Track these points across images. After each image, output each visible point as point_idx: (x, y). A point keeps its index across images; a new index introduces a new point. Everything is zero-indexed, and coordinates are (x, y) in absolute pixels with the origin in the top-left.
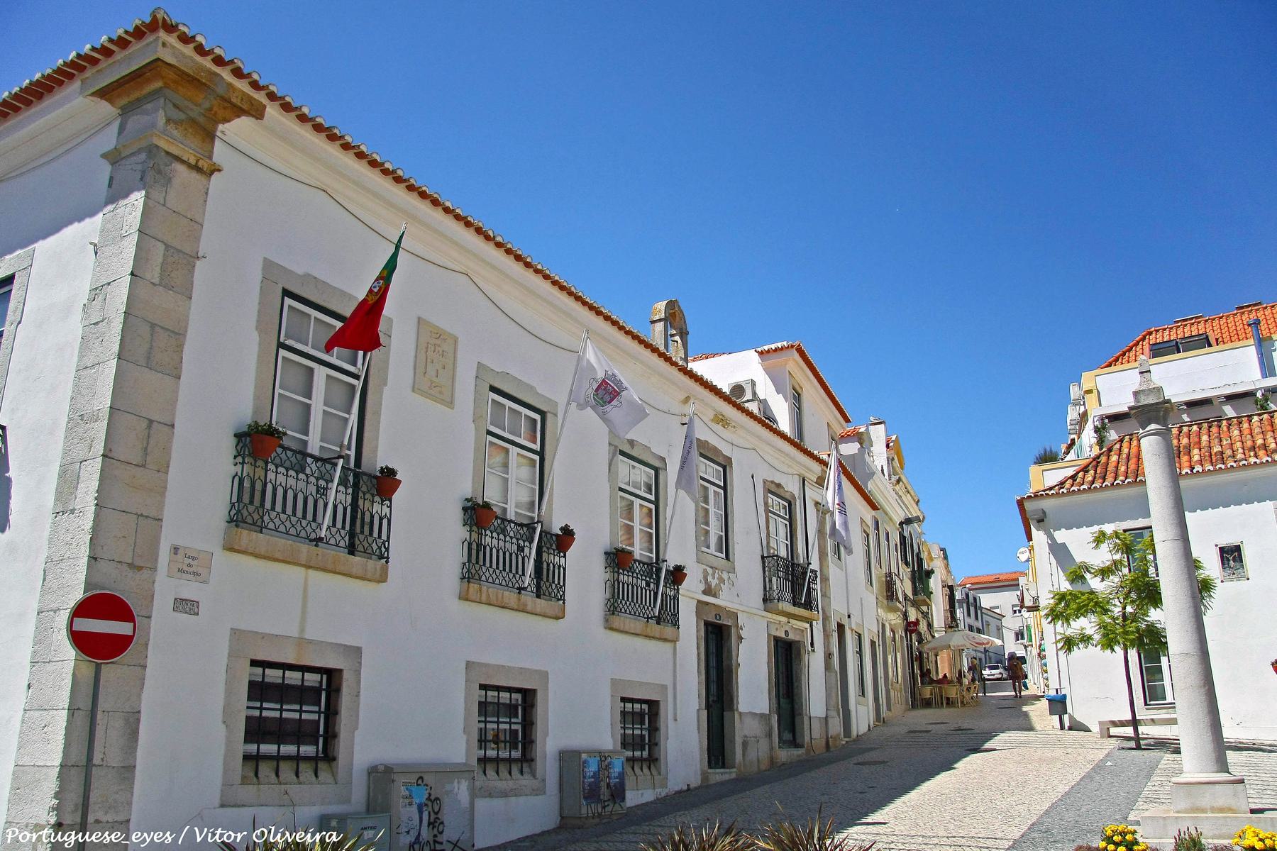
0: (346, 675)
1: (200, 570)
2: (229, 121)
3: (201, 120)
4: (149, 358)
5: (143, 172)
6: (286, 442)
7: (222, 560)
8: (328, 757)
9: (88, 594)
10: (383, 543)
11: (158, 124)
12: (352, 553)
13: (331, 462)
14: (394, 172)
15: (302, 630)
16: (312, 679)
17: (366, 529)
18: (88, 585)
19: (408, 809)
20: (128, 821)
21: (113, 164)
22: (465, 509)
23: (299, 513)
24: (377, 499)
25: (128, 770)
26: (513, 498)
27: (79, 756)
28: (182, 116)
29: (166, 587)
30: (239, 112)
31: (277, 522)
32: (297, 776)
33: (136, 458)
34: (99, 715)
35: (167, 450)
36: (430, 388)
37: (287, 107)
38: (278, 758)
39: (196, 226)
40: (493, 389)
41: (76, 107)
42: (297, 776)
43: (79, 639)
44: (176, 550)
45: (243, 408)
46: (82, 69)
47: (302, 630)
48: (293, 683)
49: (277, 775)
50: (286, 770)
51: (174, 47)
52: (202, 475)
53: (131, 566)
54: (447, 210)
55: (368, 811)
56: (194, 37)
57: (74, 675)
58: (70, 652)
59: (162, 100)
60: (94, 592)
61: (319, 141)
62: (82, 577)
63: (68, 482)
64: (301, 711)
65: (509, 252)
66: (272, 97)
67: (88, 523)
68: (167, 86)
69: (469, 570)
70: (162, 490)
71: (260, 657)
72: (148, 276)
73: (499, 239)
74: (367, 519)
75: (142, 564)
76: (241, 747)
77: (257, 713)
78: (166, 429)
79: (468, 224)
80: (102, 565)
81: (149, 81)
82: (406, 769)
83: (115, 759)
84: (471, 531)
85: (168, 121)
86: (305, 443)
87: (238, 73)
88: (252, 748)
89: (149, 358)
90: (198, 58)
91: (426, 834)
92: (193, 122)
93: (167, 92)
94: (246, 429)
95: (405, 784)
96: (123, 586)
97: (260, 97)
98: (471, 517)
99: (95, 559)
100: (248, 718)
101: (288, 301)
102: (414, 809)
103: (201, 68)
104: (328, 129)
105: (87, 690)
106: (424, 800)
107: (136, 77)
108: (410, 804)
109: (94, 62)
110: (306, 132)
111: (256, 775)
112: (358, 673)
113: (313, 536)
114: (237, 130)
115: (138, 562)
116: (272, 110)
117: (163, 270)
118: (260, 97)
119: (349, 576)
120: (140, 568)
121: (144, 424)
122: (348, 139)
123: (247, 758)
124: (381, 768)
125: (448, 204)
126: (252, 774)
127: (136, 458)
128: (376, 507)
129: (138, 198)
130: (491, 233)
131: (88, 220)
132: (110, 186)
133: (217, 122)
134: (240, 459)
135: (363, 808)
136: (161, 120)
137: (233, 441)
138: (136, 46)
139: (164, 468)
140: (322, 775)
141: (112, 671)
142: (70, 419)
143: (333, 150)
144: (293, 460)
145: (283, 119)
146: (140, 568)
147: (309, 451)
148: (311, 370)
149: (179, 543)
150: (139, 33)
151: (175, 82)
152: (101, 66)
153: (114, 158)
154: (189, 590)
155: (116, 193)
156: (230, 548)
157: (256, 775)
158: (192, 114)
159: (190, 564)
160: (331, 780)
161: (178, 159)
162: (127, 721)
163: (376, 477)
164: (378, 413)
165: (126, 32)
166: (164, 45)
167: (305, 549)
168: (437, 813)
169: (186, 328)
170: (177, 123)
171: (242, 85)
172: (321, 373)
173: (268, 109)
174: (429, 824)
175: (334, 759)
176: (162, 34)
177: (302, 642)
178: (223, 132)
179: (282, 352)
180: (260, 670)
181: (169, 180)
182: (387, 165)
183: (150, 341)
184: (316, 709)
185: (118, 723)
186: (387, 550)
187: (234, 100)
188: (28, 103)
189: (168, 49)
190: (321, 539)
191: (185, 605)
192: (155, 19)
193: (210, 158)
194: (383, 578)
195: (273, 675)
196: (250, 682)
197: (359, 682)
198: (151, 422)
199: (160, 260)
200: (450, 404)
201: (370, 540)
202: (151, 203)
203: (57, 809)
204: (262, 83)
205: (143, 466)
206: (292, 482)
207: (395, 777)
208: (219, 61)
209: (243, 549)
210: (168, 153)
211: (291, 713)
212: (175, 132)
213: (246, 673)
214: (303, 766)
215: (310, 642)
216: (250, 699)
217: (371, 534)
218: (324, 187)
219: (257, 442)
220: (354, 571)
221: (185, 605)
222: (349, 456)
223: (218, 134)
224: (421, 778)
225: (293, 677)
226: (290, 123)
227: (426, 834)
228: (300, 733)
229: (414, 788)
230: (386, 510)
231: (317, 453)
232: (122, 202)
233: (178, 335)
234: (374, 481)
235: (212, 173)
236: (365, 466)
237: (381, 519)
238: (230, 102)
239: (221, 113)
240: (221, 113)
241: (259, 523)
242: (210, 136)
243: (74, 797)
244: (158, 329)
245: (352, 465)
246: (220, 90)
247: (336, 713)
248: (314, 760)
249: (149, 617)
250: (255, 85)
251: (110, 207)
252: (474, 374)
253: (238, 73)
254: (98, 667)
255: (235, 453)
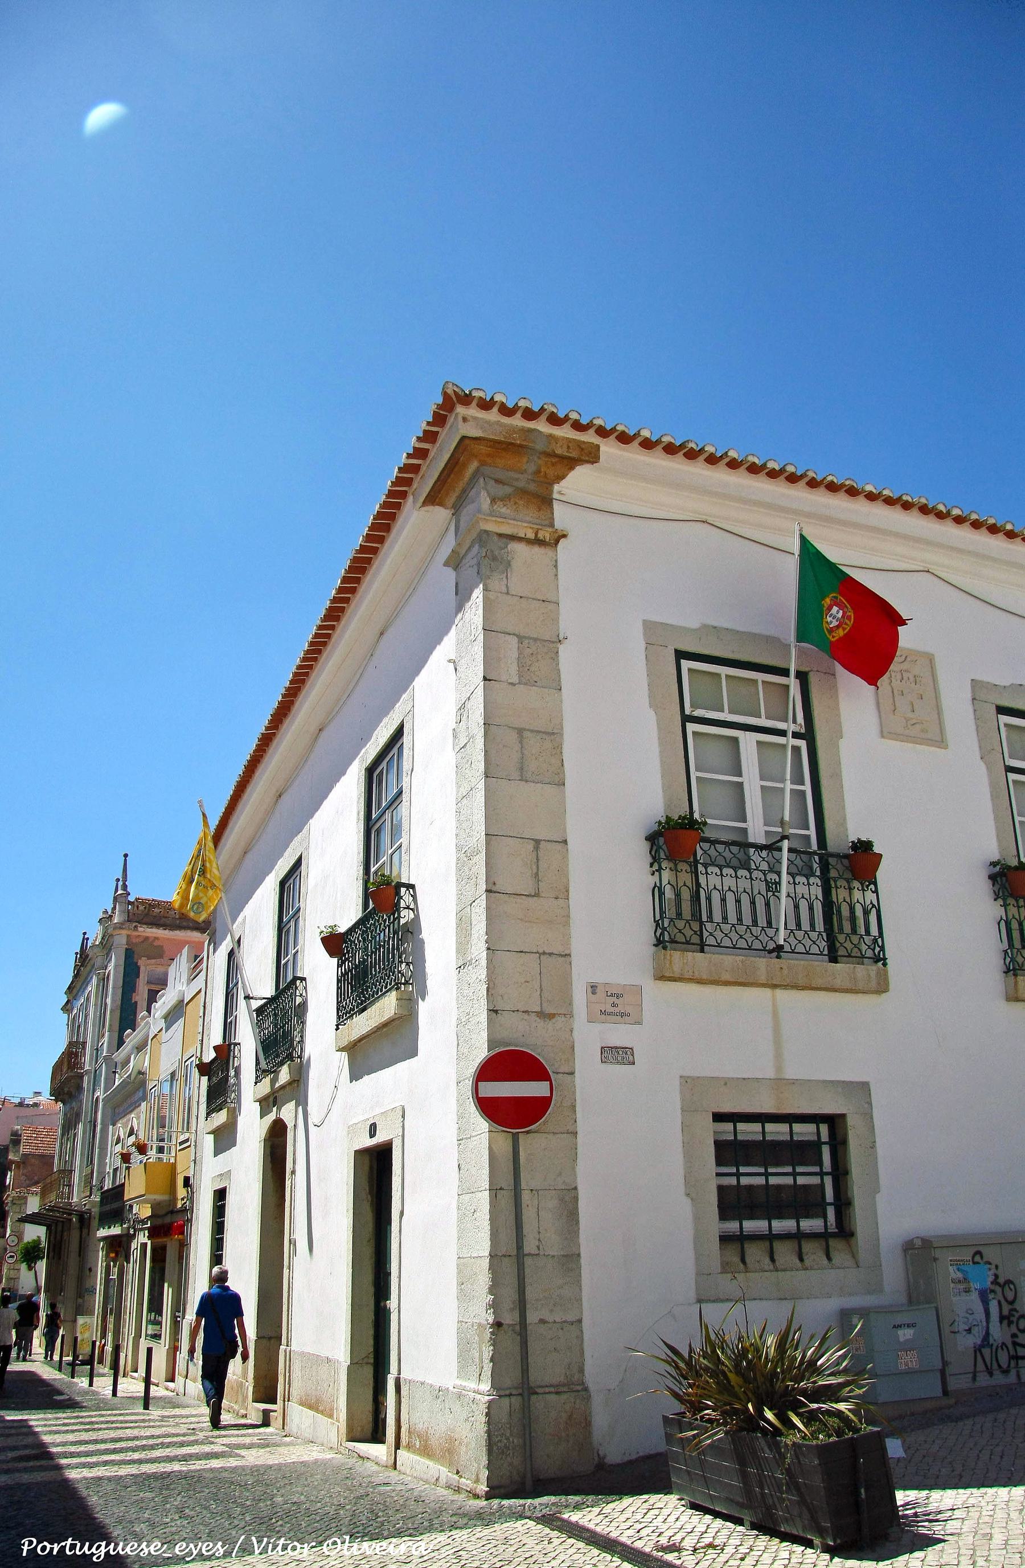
0: (850, 1121)
1: (628, 1009)
2: (563, 477)
3: (532, 487)
4: (522, 769)
5: (479, 564)
6: (708, 833)
7: (657, 996)
8: (845, 1232)
9: (493, 1053)
10: (875, 941)
11: (488, 511)
12: (834, 959)
13: (773, 847)
14: (782, 471)
15: (779, 1068)
16: (804, 1131)
17: (847, 927)
18: (491, 1043)
19: (965, 1297)
20: (580, 1321)
21: (456, 568)
22: (992, 878)
23: (747, 920)
24: (856, 884)
25: (571, 1261)
26: (760, 802)
27: (508, 1246)
28: (508, 490)
29: (588, 1036)
30: (571, 463)
31: (719, 935)
32: (801, 1259)
33: (526, 886)
34: (526, 1196)
35: (563, 872)
36: (906, 727)
37: (624, 438)
38: (770, 1238)
39: (551, 606)
40: (1002, 710)
41: (421, 524)
42: (801, 1259)
43: (489, 1107)
44: (593, 988)
45: (651, 801)
46: (409, 482)
47: (779, 1068)
48: (750, 1138)
49: (773, 1260)
50: (785, 1252)
51: (475, 418)
52: (612, 897)
53: (541, 1015)
54: (871, 497)
55: (910, 1302)
56: (900, 497)
57: (490, 1148)
58: (482, 1125)
59: (482, 480)
60: (497, 1050)
61: (677, 465)
62: (484, 1035)
63: (463, 926)
64: (794, 1174)
65: (976, 525)
66: (603, 432)
67: (483, 974)
68: (483, 463)
69: (1012, 960)
70: (566, 919)
71: (727, 1108)
72: (504, 678)
73: (956, 512)
74: (845, 911)
75: (553, 1012)
76: (715, 1226)
77: (733, 1181)
78: (559, 846)
79: (907, 506)
80: (505, 1019)
81: (465, 466)
82: (953, 1243)
83: (554, 1245)
84: (1005, 905)
85: (493, 500)
86: (745, 831)
87: (554, 420)
88: (733, 1226)
89: (522, 769)
90: (506, 420)
91: (998, 1333)
92: (523, 493)
93: (487, 470)
94: (656, 827)
95: (954, 1263)
96: (534, 1038)
97: (590, 437)
98: (1003, 887)
99: (496, 1012)
100: (721, 1189)
101: (685, 664)
102: (975, 1296)
103: (513, 430)
104: (682, 446)
105: (507, 1167)
106: (988, 1284)
107: (453, 466)
108: (967, 1291)
109: (415, 469)
110: (657, 460)
111: (743, 1260)
112: (868, 1116)
113: (771, 946)
114: (577, 484)
115: (549, 1009)
116: (608, 449)
117: (521, 665)
118: (590, 437)
119: (835, 990)
120: (551, 1016)
121: (531, 846)
122: (710, 449)
123: (725, 1239)
124: (918, 1243)
125: (869, 488)
126: (736, 1259)
127: (526, 886)
128: (857, 895)
129: (478, 594)
130: (941, 507)
131: (446, 639)
132: (457, 594)
133: (551, 484)
134: (656, 867)
135: (903, 1299)
136: (485, 502)
137: (646, 846)
138: (443, 433)
139: (563, 893)
140: (838, 1258)
141: (534, 1143)
142: (458, 859)
143: (698, 470)
144: (727, 854)
145: (626, 454)
146: (551, 1016)
147: (751, 840)
148: (735, 740)
149: (599, 979)
150: (439, 419)
151: (489, 455)
152: (423, 469)
153: (455, 561)
154: (619, 1035)
155: (462, 596)
156: (661, 977)
157: (743, 1260)
158: (521, 484)
159: (615, 1004)
160: (850, 1262)
161: (513, 538)
162: (562, 1200)
163: (846, 856)
164: (837, 776)
165: (428, 423)
166: (465, 420)
167: (762, 964)
168: (1012, 1303)
169: (561, 724)
170: (505, 499)
171: (565, 432)
172: (748, 741)
173: (603, 449)
174: (1002, 1318)
175: (852, 1234)
176: (460, 410)
177: (780, 1083)
178: (560, 493)
179: (691, 727)
180: (730, 1126)
181: (509, 564)
182: (771, 465)
183: (519, 751)
184: (817, 1169)
185: (551, 1203)
186: (882, 948)
187: (559, 451)
188: (381, 540)
189: (470, 422)
190: (779, 948)
191: (617, 1055)
192: (445, 395)
193: (552, 525)
194: (882, 987)
195: (749, 1131)
196: (717, 1143)
197: (872, 1128)
198: (537, 842)
199: (515, 654)
200: (941, 742)
201: (855, 939)
202: (492, 596)
203: (494, 1306)
204: (584, 421)
205: (537, 895)
206: (729, 882)
207: (938, 1253)
208: (529, 415)
209: (677, 975)
210: (500, 535)
211: (780, 1178)
212: (503, 510)
213: (707, 1132)
214: (808, 1247)
215: (794, 1082)
216: (719, 1162)
217: (854, 930)
218: (704, 518)
219: (674, 840)
220: (838, 983)
221: (617, 1055)
222: (808, 837)
223: (555, 496)
224: (979, 1253)
225: (777, 1131)
226: (633, 454)
227: (998, 1333)
228: (804, 1202)
229: (969, 1268)
230: (870, 896)
231: (762, 841)
232: (468, 605)
233: (553, 735)
234: (846, 862)
235: (557, 541)
236: (832, 845)
237: (866, 913)
238: (554, 455)
239: (551, 472)
240: (551, 472)
241: (696, 939)
242: (546, 502)
243: (510, 1293)
244: (527, 734)
245: (814, 846)
246: (540, 446)
247: (846, 1172)
248: (823, 1237)
249: (572, 1073)
250: (577, 426)
251: (460, 616)
252: (969, 696)
253: (554, 420)
254: (515, 1139)
255: (650, 860)
